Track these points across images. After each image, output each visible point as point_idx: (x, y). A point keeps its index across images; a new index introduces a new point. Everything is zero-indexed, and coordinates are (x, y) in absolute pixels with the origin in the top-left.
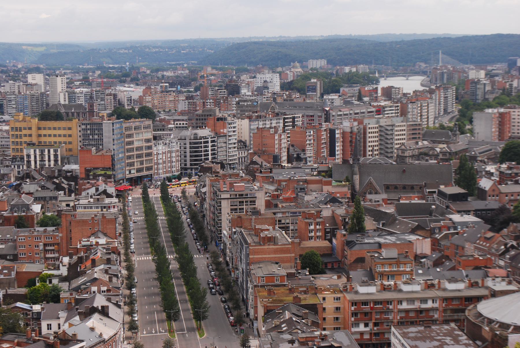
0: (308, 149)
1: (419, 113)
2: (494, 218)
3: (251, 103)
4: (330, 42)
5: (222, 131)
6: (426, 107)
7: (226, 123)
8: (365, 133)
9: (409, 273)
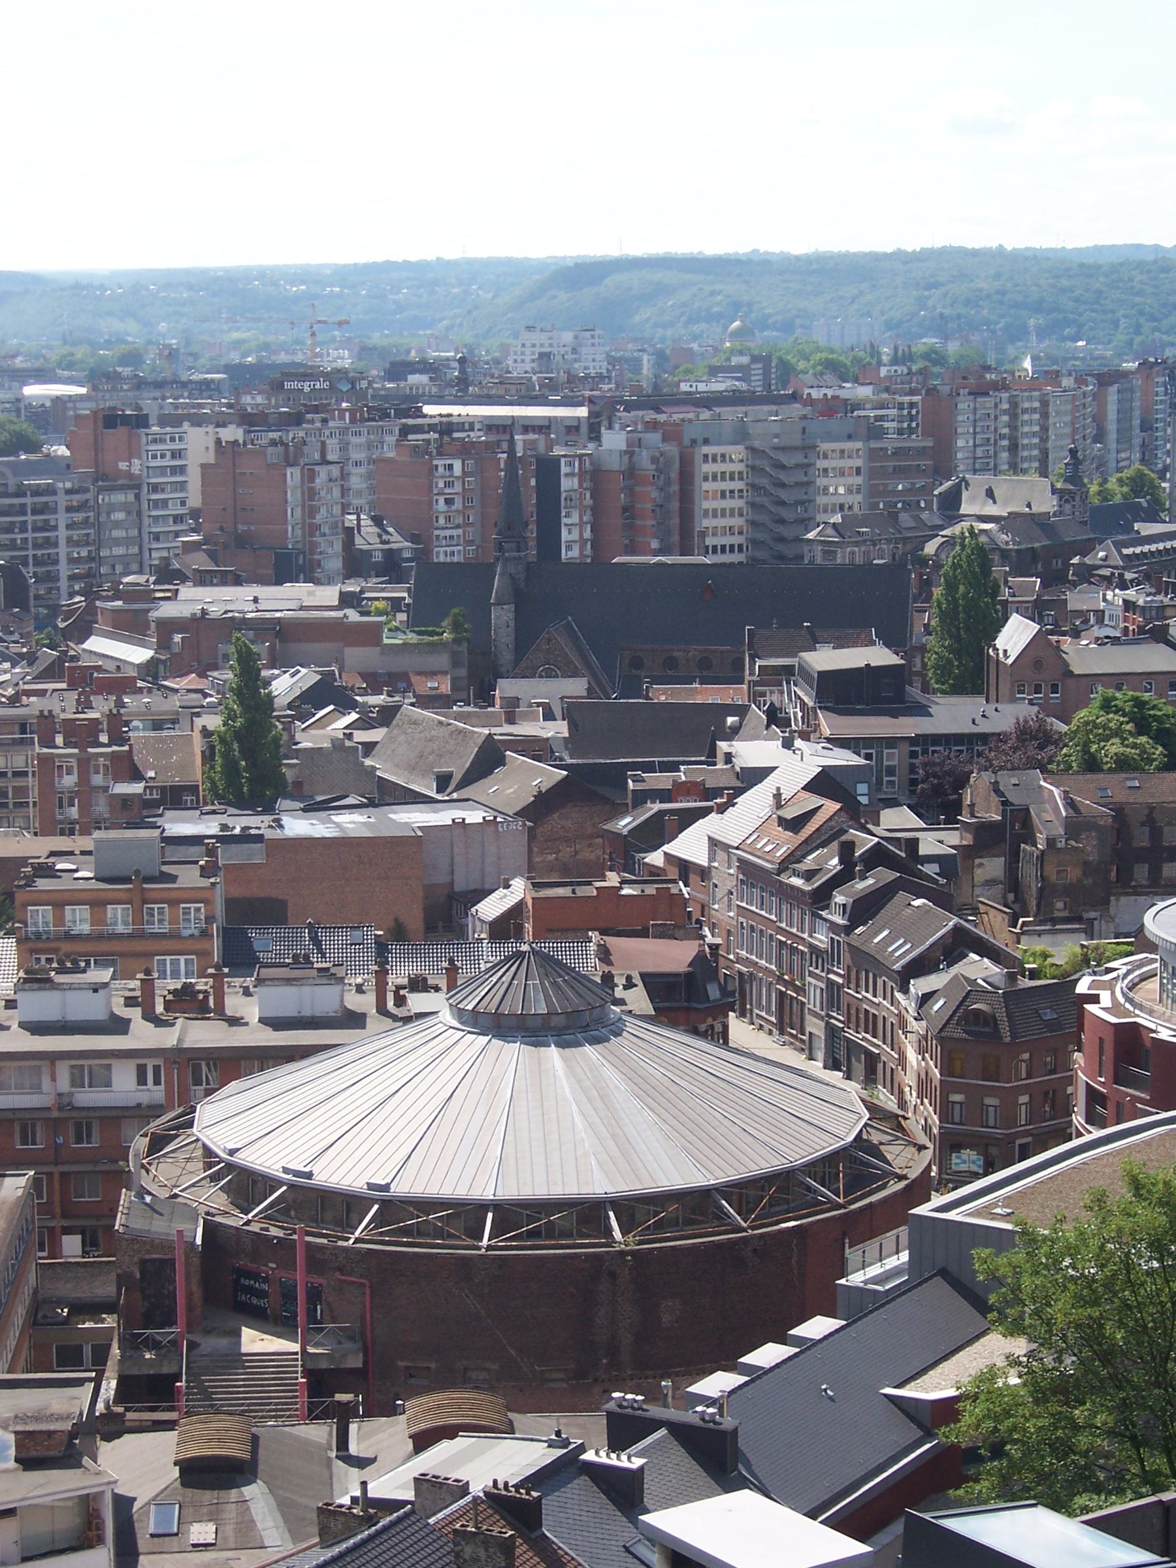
0: (442, 533)
1: (1002, 437)
2: (412, 638)
3: (326, 385)
4: (905, 263)
5: (123, 466)
6: (1036, 416)
7: (139, 436)
8: (686, 477)
9: (189, 944)
